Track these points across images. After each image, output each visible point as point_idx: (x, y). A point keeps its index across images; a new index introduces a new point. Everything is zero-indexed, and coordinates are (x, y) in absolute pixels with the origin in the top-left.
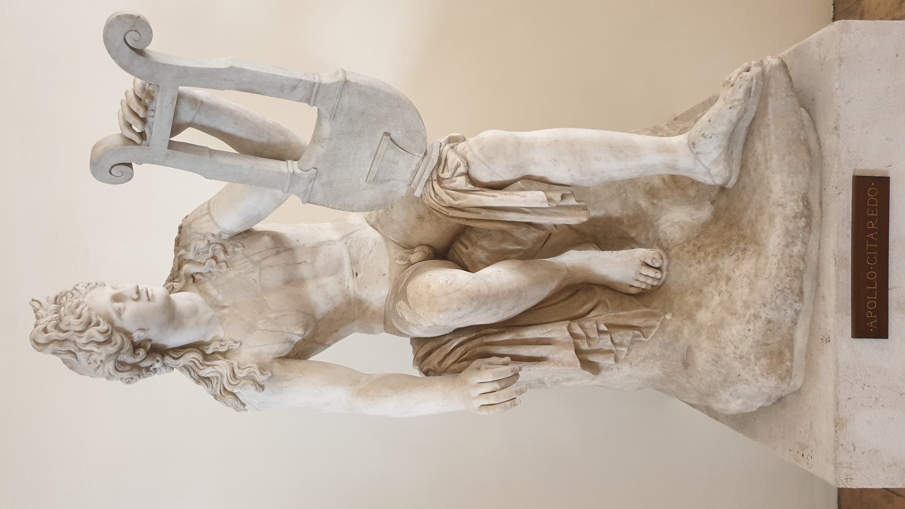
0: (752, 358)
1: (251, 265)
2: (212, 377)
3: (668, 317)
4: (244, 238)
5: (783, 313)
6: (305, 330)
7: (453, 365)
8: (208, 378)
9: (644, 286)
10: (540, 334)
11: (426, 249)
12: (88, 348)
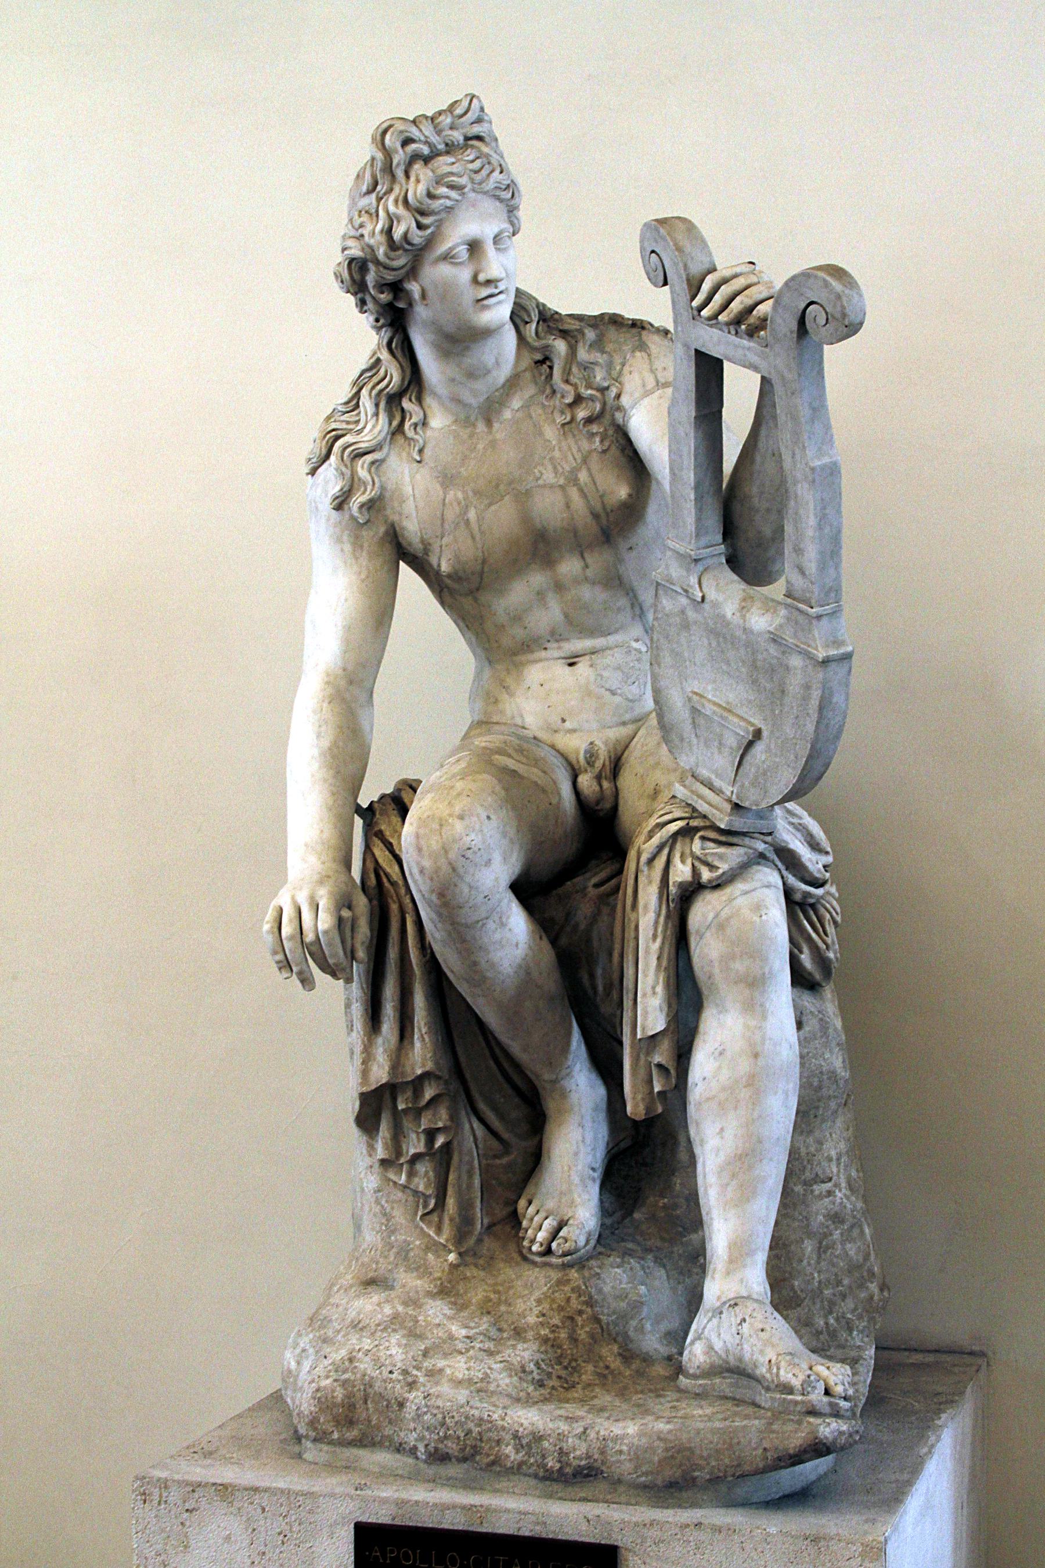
0: (346, 1376)
1: (568, 468)
3: (452, 1257)
4: (623, 450)
5: (412, 1425)
6: (449, 576)
8: (357, 406)
9: (525, 1224)
11: (607, 805)
12: (381, 213)
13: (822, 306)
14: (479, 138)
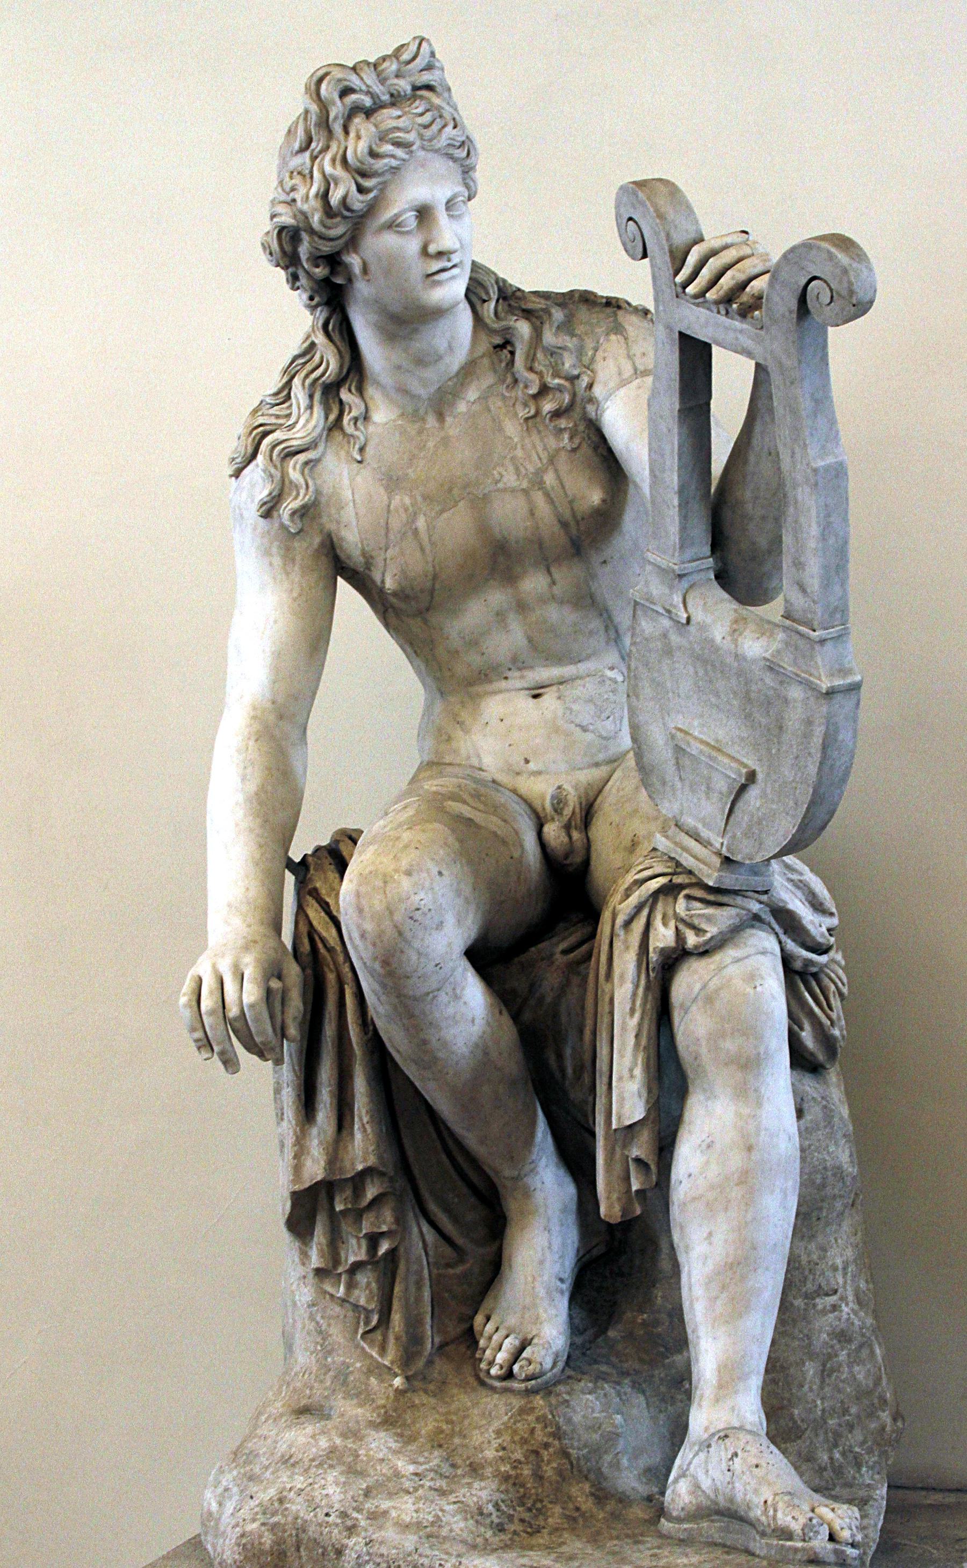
0: (275, 1519)
2: (291, 405)
3: (398, 1382)
4: (595, 449)
6: (395, 594)
7: (306, 922)
8: (288, 397)
9: (482, 1343)
10: (359, 1109)
11: (578, 859)
12: (316, 174)
13: (825, 282)
14: (429, 88)
